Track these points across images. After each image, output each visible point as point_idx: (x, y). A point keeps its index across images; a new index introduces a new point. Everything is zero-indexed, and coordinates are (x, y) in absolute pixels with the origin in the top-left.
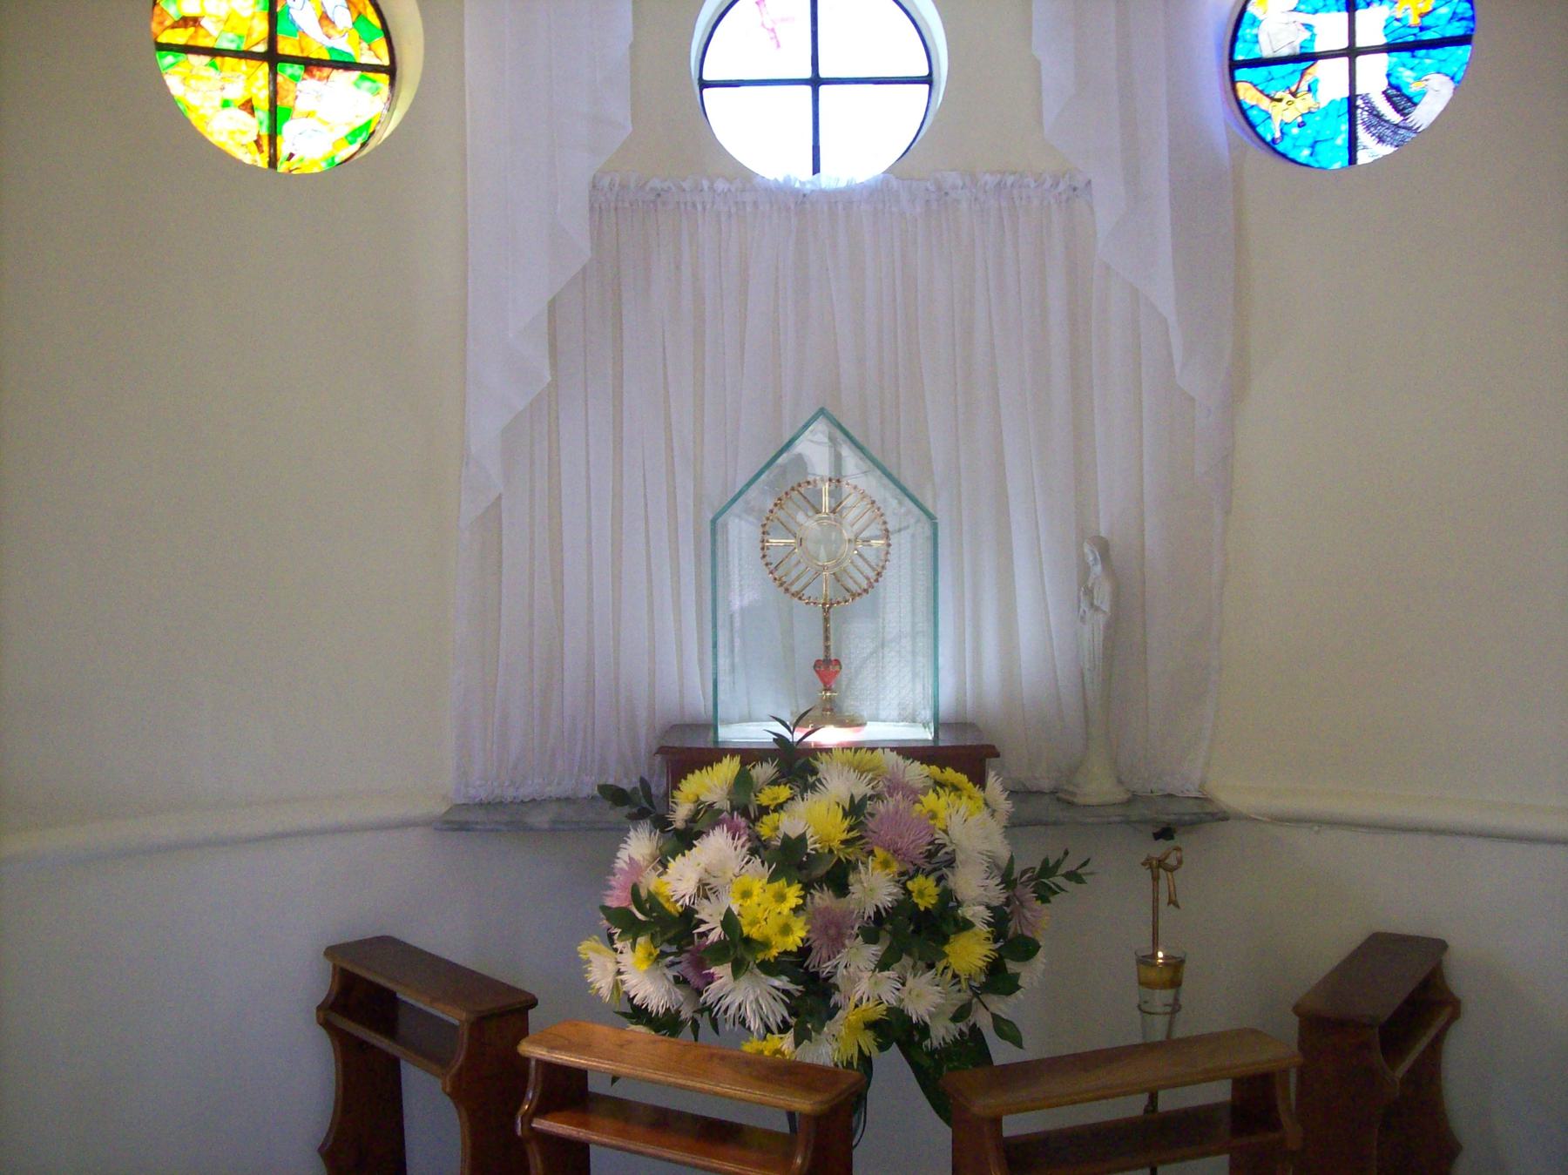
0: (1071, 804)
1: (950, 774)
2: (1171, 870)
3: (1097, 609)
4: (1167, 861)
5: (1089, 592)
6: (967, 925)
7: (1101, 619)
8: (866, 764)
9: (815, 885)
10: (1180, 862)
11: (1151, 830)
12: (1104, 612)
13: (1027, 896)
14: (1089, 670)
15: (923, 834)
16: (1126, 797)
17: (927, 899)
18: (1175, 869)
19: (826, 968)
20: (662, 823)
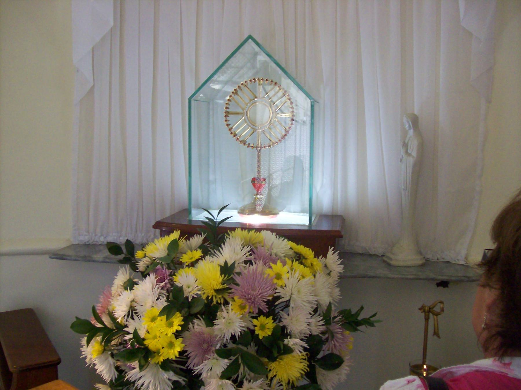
0: (389, 265)
1: (302, 249)
2: (437, 314)
3: (409, 154)
4: (434, 309)
5: (405, 145)
6: (288, 350)
7: (411, 161)
8: (253, 241)
9: (198, 316)
10: (442, 310)
11: (435, 282)
12: (413, 157)
13: (336, 331)
14: (404, 189)
15: (268, 289)
16: (420, 262)
17: (266, 330)
18: (439, 314)
19: (197, 370)
20: (134, 268)
